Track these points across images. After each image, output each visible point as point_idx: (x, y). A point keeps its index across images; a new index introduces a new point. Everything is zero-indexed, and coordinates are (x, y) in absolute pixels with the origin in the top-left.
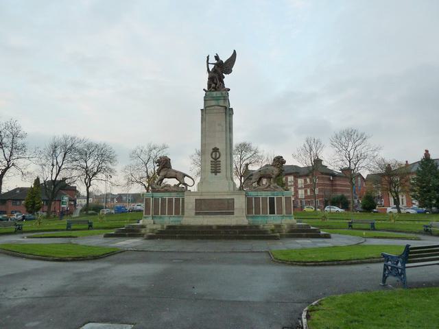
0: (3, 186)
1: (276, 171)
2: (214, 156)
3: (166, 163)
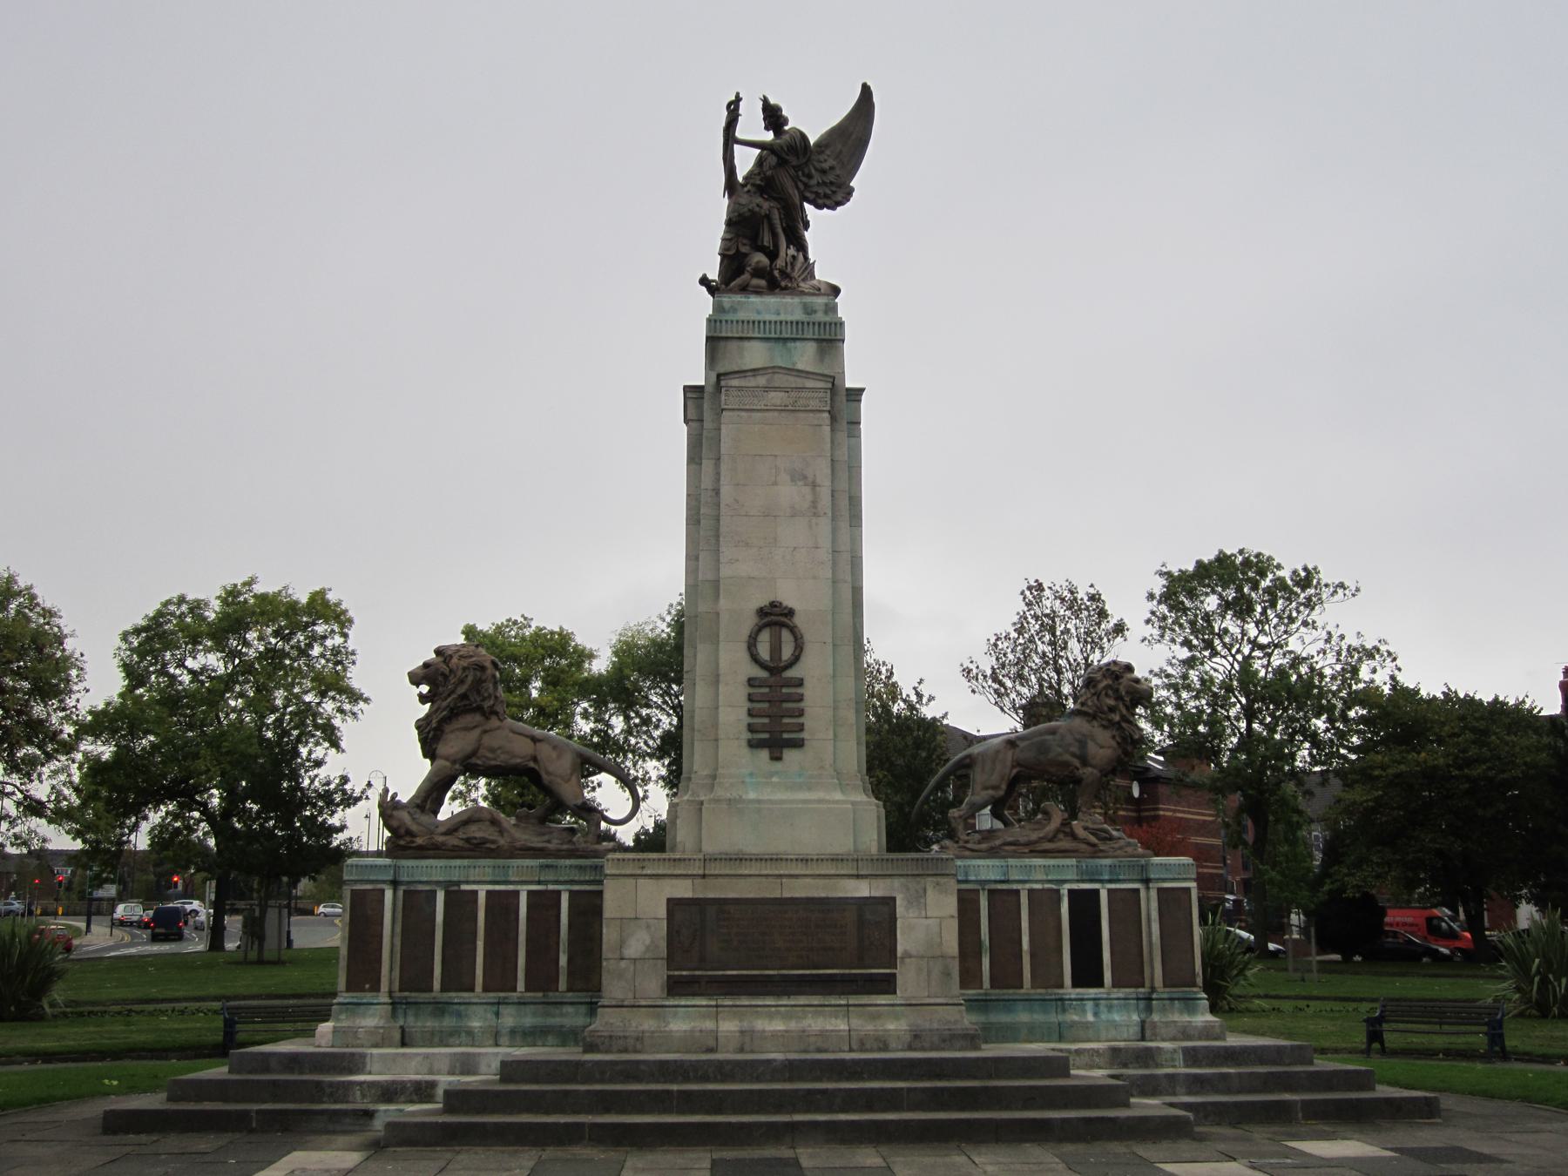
0: (422, 715)
1: (1102, 745)
2: (764, 652)
3: (478, 685)
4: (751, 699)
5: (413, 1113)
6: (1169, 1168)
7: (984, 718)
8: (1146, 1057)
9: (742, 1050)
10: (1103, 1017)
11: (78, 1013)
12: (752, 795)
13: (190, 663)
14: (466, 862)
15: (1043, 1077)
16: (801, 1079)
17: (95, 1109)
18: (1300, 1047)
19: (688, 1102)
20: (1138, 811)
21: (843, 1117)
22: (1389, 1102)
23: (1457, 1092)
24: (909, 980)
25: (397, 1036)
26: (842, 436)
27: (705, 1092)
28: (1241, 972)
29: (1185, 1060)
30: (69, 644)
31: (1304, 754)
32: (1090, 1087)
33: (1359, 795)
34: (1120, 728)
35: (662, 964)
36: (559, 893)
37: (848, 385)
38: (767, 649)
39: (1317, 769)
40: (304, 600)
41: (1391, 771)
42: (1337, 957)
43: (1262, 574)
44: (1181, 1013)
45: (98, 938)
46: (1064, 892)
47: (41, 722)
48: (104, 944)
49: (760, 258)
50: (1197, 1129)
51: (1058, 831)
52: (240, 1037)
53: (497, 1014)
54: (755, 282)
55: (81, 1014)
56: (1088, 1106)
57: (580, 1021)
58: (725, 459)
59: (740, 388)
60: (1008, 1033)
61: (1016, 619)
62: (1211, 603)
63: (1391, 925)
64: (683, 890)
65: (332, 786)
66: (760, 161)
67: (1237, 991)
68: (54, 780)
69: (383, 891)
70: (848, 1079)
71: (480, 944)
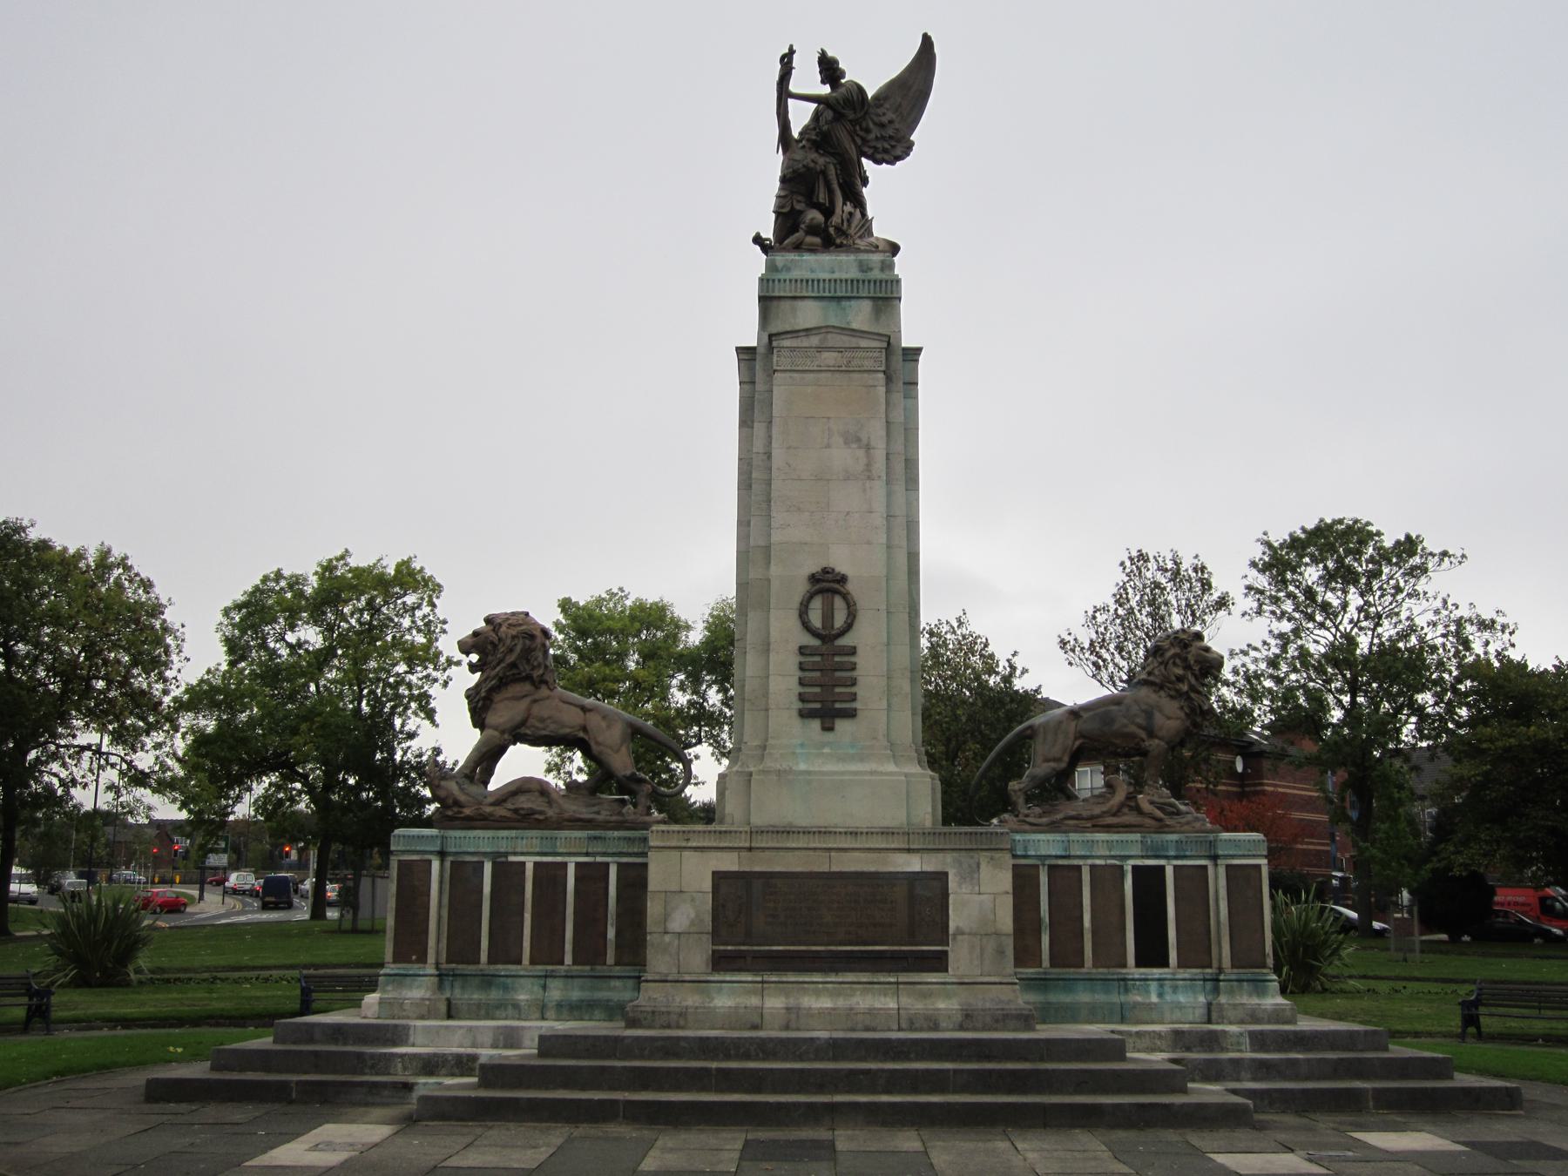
0: (472, 684)
1: (1170, 716)
2: (816, 619)
3: (527, 653)
4: (802, 667)
5: (449, 1087)
6: (1221, 1159)
7: (1070, 686)
8: (1211, 1041)
9: (787, 1028)
10: (1168, 998)
11: (162, 979)
12: (802, 767)
14: (513, 833)
15: (1096, 1060)
16: (845, 1058)
17: (139, 1078)
18: (1375, 1032)
19: (728, 1080)
20: (1242, 786)
21: (885, 1098)
22: (1467, 1091)
23: (1549, 1081)
24: (961, 959)
25: (443, 1008)
26: (897, 397)
27: (744, 1070)
28: (1335, 952)
29: (1252, 1044)
30: (169, 615)
31: (1408, 732)
32: (1144, 1072)
33: (1467, 769)
34: (1189, 698)
35: (707, 939)
36: (607, 865)
37: (904, 345)
38: (826, 616)
39: (1424, 744)
40: (391, 571)
41: (1499, 744)
42: (1444, 937)
43: (1363, 542)
44: (1250, 995)
45: (211, 906)
46: (1128, 869)
47: (143, 692)
48: (214, 912)
49: (814, 216)
50: (1257, 1117)
51: (1122, 805)
52: (314, 1006)
53: (544, 987)
54: (809, 239)
55: (168, 981)
56: (1143, 1091)
57: (627, 995)
58: (776, 421)
59: (792, 349)
60: (1069, 1014)
62: (1312, 574)
63: (1502, 904)
65: (424, 758)
66: (816, 116)
67: (1330, 971)
68: (163, 750)
69: (430, 862)
70: (894, 1059)
71: (528, 917)
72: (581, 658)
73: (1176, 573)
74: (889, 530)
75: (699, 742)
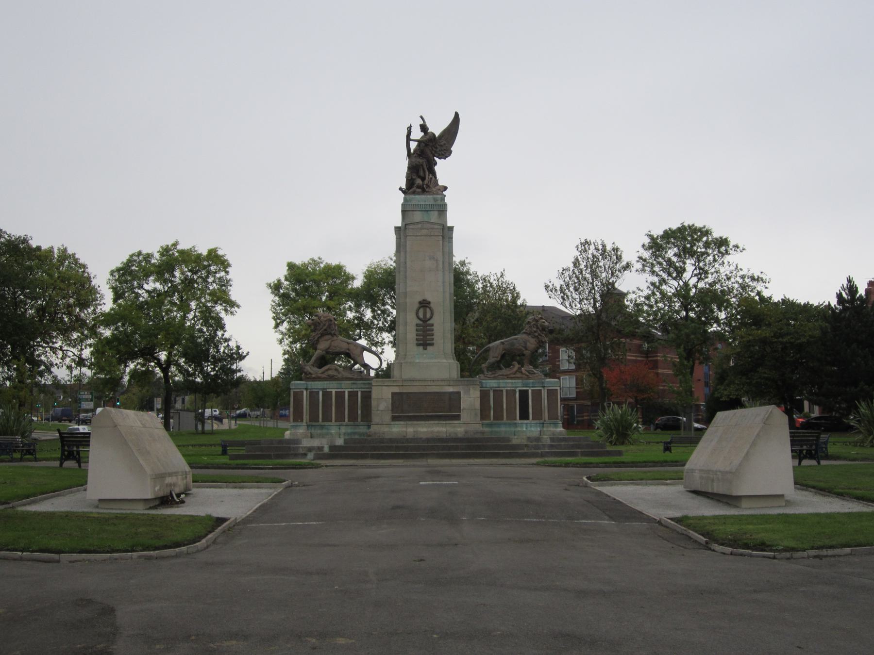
2: (421, 315)
3: (329, 326)
13: (146, 286)
19: (397, 448)
20: (647, 357)
24: (465, 416)
40: (205, 253)
49: (419, 181)
61: (573, 260)
62: (671, 253)
64: (396, 390)
66: (418, 146)
72: (297, 294)
73: (604, 250)
74: (444, 286)
75: (360, 338)
